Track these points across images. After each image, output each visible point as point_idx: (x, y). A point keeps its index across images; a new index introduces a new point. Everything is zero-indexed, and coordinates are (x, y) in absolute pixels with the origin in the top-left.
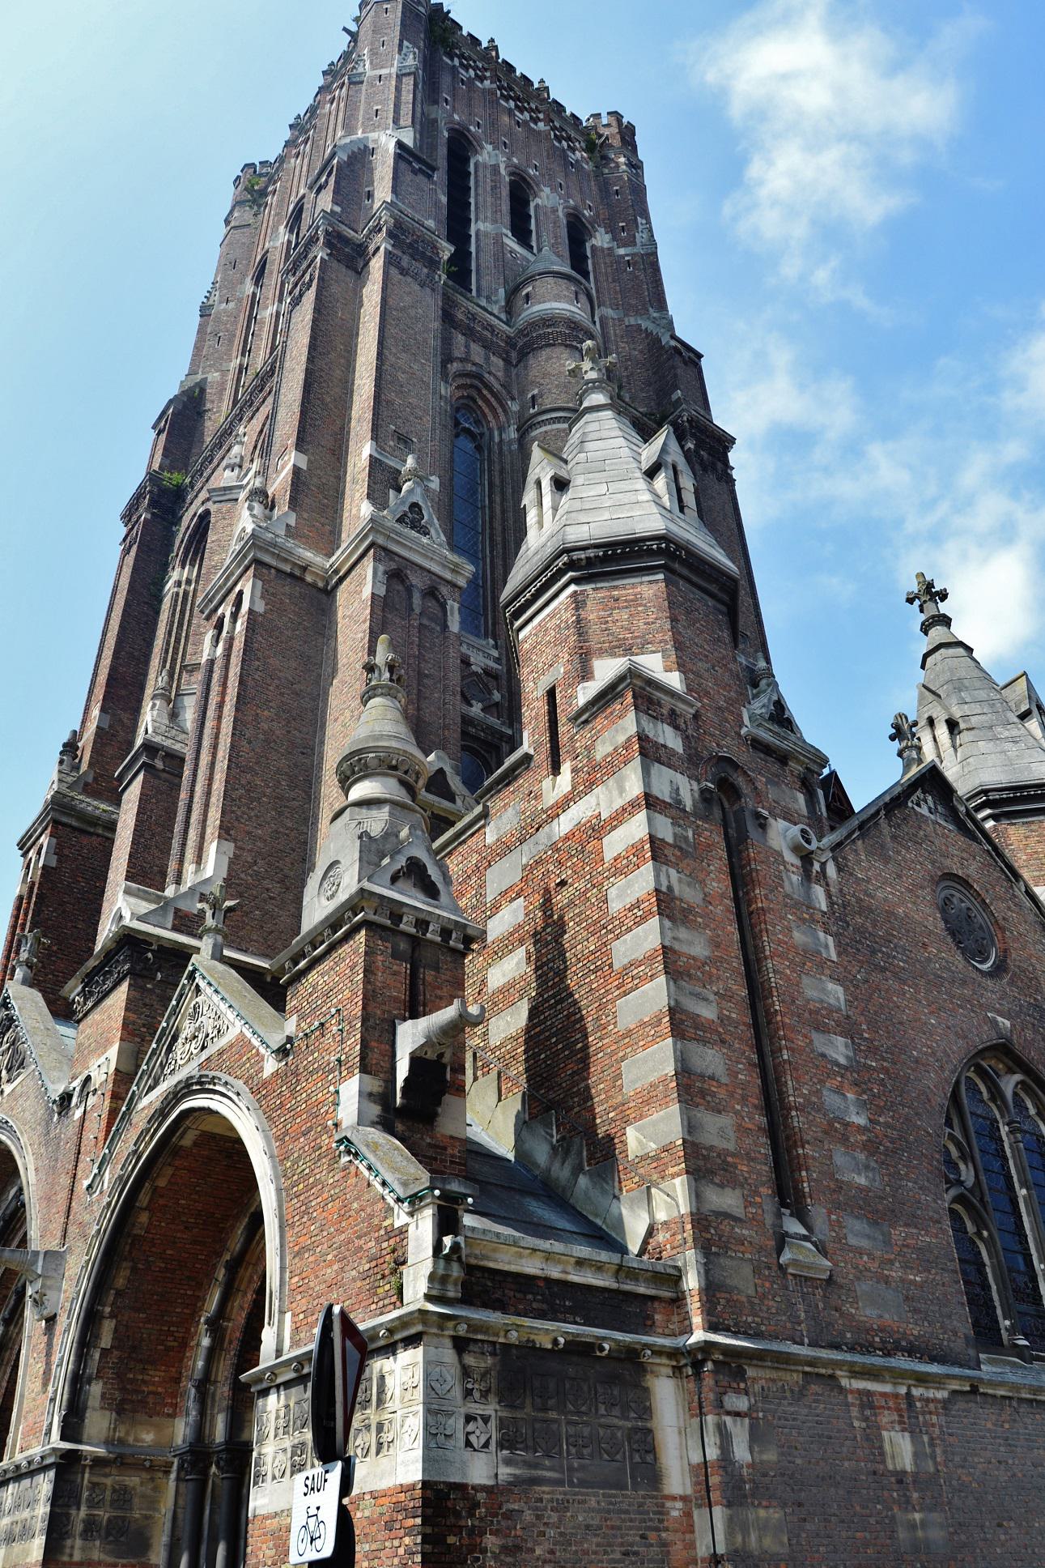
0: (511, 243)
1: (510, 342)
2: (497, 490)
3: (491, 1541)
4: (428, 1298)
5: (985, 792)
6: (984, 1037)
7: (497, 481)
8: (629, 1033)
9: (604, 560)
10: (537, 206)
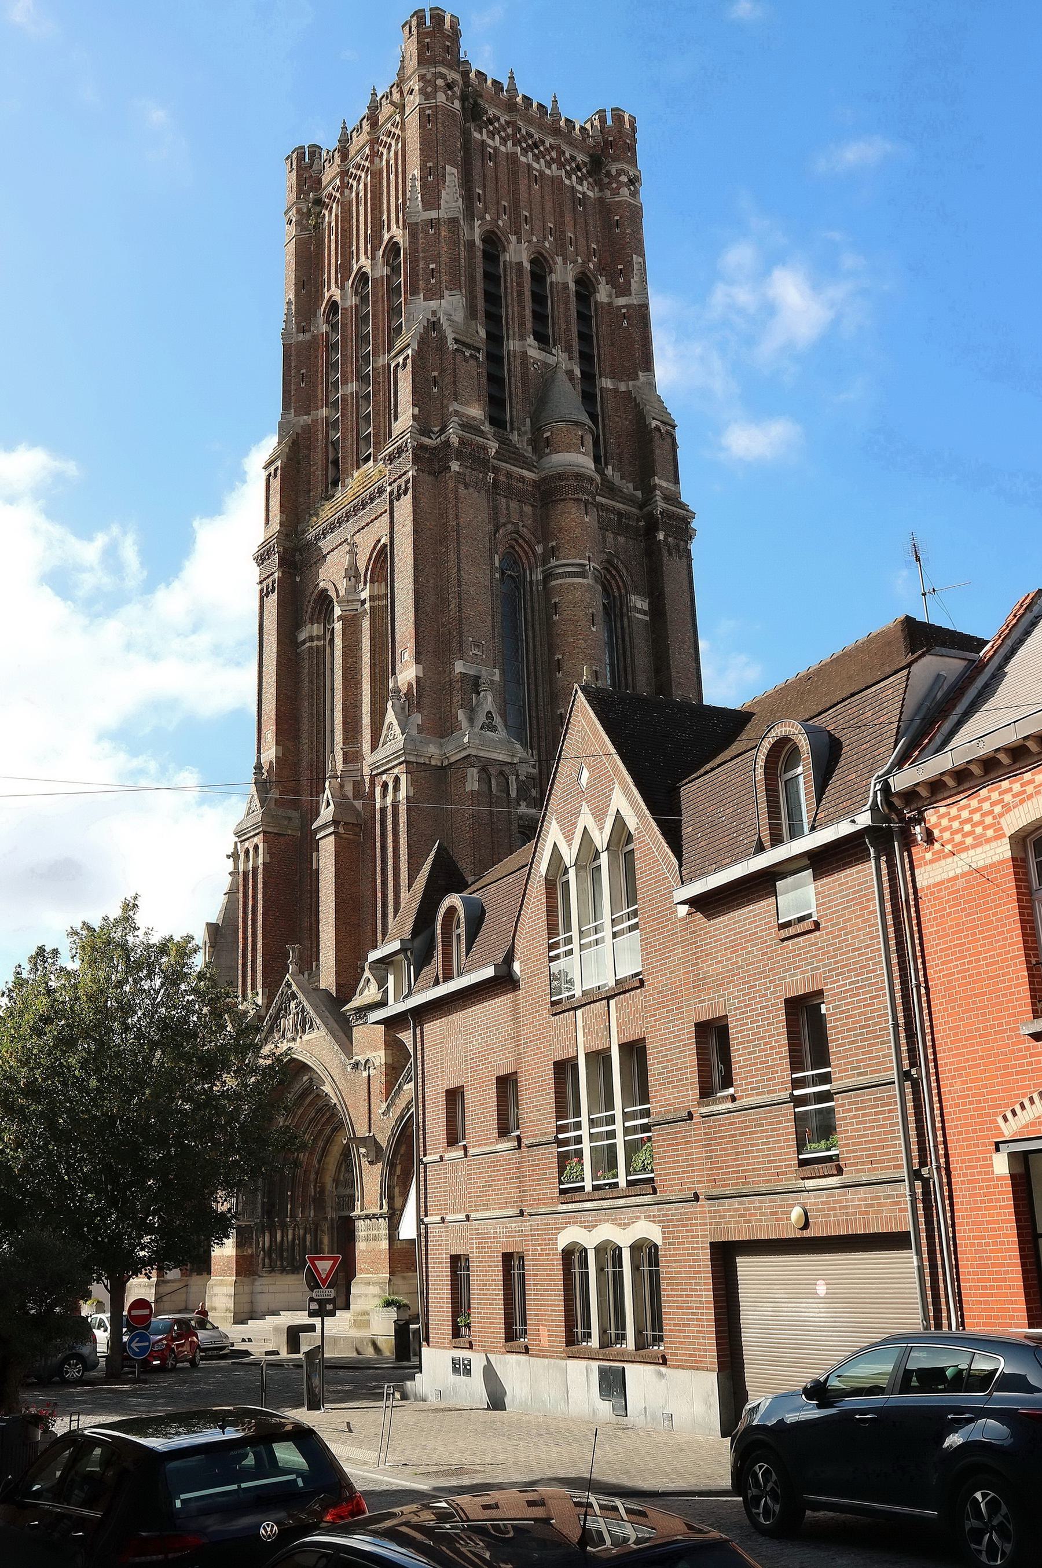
7: (529, 618)
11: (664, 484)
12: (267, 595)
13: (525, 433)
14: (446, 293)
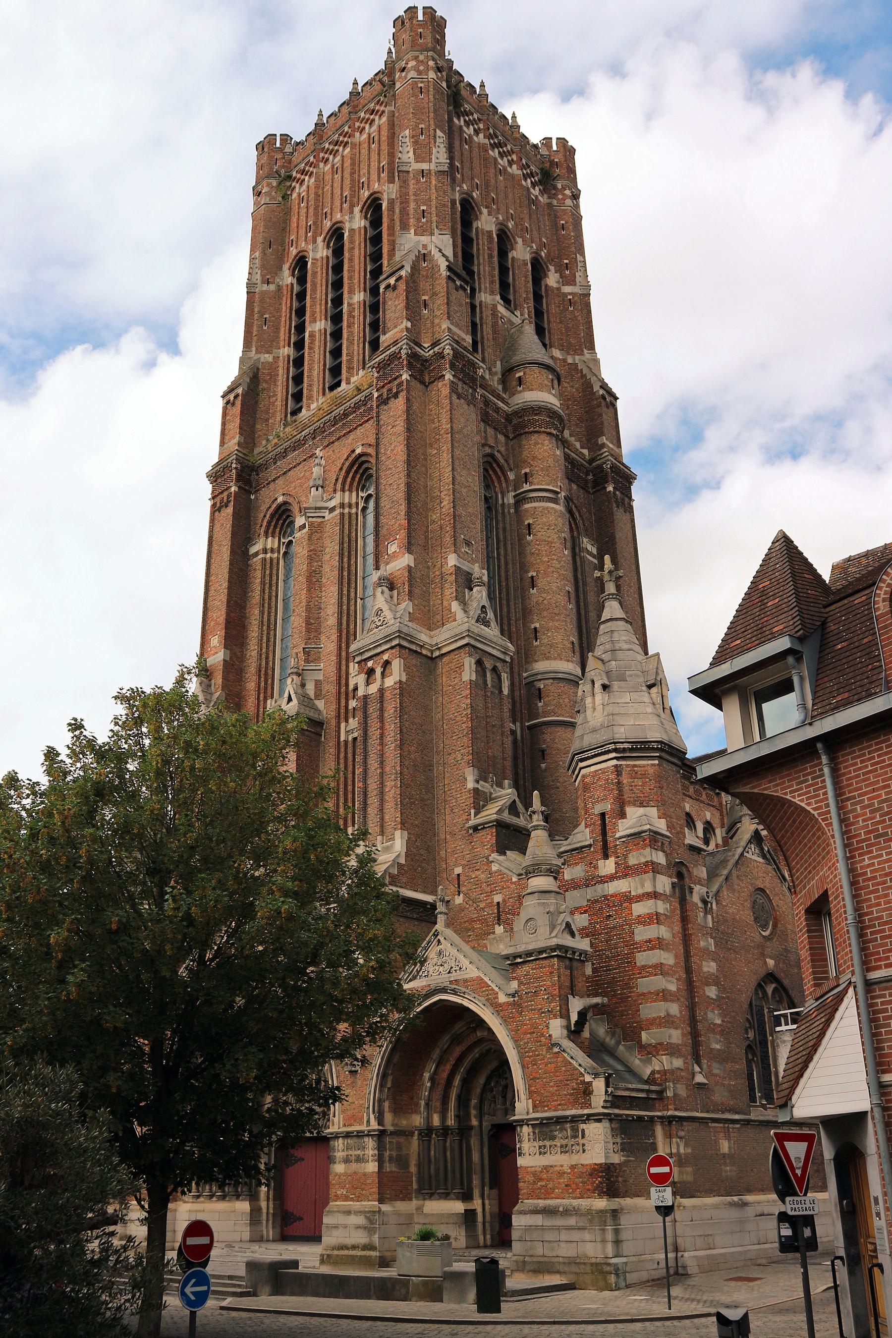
0: (501, 309)
1: (508, 418)
2: (502, 544)
3: (620, 1179)
6: (762, 973)
7: (501, 537)
8: (643, 994)
9: (631, 750)
10: (513, 258)
11: (611, 445)
12: (219, 510)
13: (496, 373)
14: (436, 231)
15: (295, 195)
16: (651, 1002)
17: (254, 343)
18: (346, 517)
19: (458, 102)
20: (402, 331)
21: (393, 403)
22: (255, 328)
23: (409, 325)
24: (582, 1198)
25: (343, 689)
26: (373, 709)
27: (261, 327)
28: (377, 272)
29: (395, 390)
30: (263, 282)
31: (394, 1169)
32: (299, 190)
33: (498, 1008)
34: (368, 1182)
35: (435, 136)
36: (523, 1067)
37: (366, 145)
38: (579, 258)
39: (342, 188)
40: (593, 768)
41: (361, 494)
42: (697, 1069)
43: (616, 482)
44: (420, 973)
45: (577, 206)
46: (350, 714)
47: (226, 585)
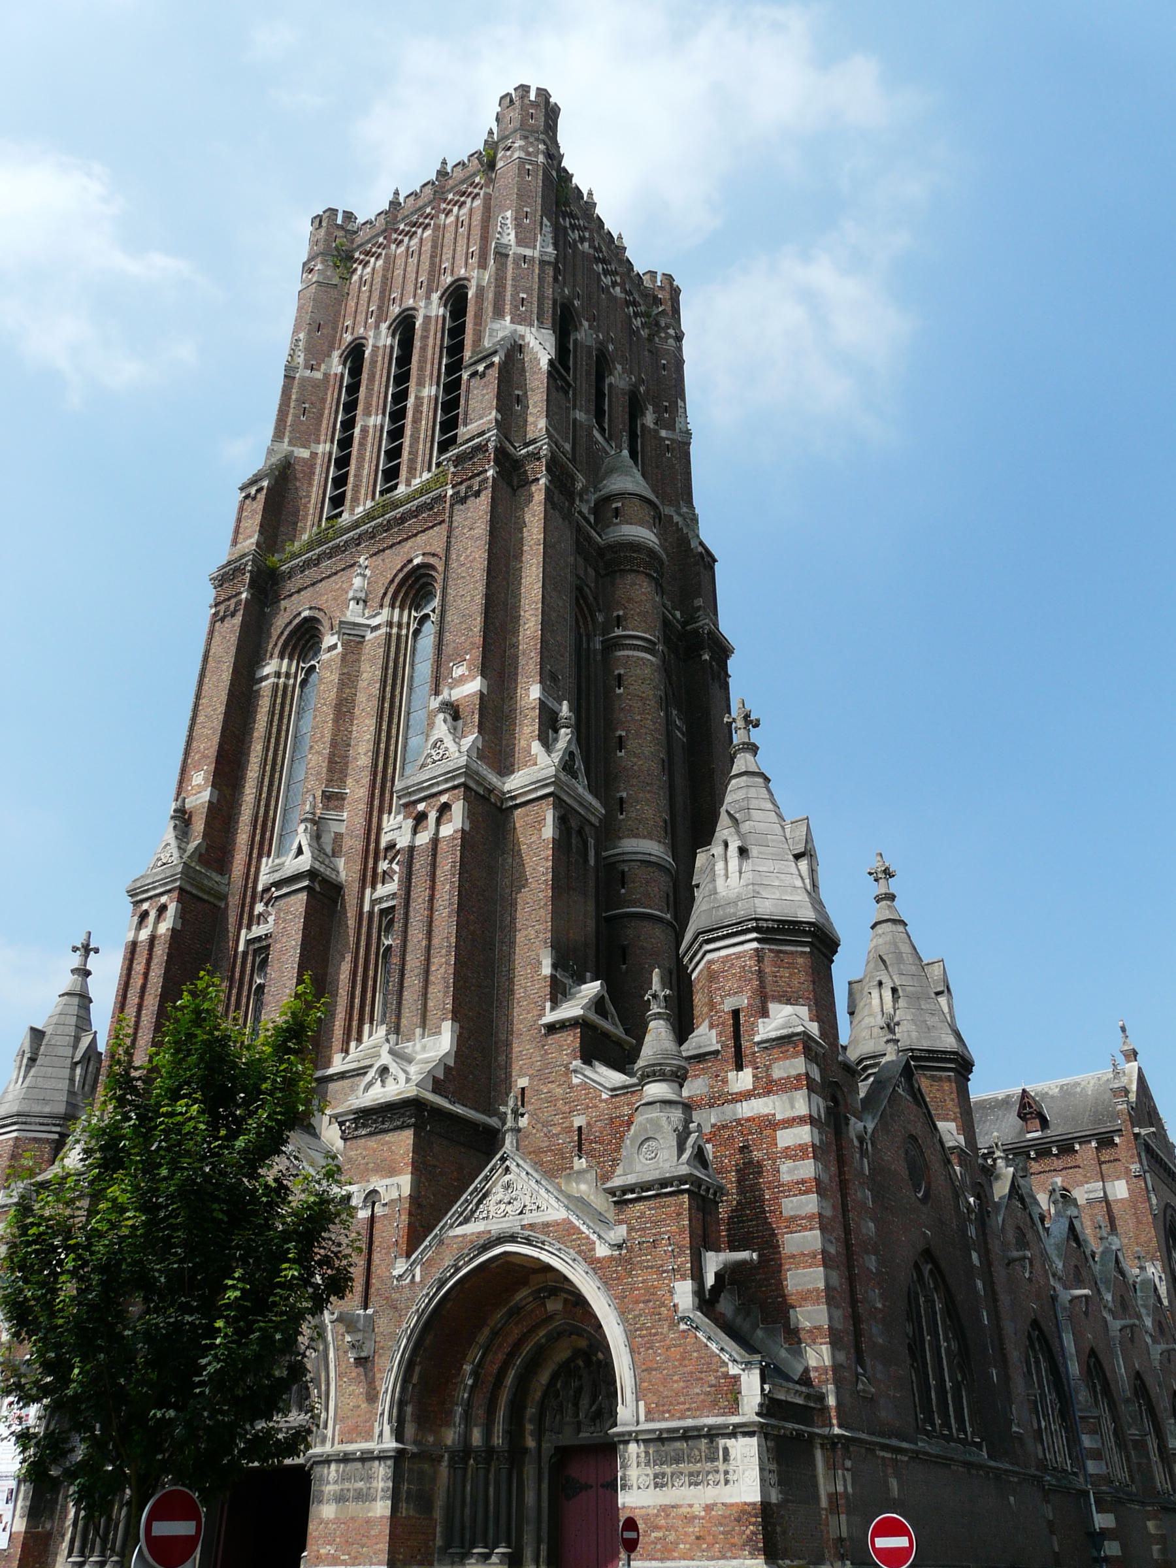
1: (601, 551)
3: (778, 1529)
4: (758, 1414)
5: (912, 1050)
10: (611, 385)
12: (222, 620)
15: (355, 278)
16: (804, 1268)
17: (287, 434)
18: (394, 638)
19: (562, 202)
20: (490, 422)
21: (471, 502)
22: (290, 418)
23: (499, 417)
24: (724, 1557)
25: (372, 846)
26: (421, 864)
27: (296, 416)
28: (455, 367)
29: (476, 488)
30: (306, 368)
31: (412, 1513)
32: (361, 272)
33: (595, 1265)
34: (373, 1533)
35: (541, 223)
36: (632, 1351)
37: (453, 229)
38: (680, 403)
39: (417, 273)
40: (723, 953)
41: (414, 613)
42: (860, 1370)
43: (712, 651)
44: (476, 1215)
45: (680, 349)
46: (380, 879)
47: (222, 709)
